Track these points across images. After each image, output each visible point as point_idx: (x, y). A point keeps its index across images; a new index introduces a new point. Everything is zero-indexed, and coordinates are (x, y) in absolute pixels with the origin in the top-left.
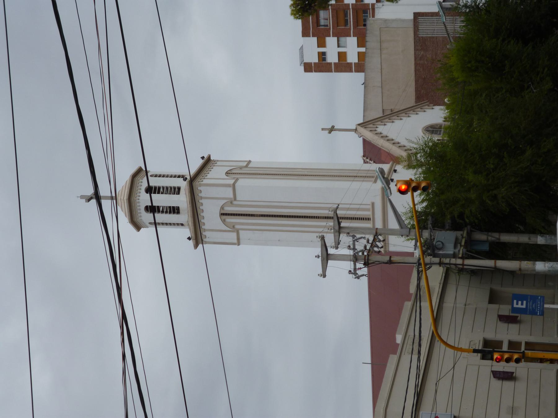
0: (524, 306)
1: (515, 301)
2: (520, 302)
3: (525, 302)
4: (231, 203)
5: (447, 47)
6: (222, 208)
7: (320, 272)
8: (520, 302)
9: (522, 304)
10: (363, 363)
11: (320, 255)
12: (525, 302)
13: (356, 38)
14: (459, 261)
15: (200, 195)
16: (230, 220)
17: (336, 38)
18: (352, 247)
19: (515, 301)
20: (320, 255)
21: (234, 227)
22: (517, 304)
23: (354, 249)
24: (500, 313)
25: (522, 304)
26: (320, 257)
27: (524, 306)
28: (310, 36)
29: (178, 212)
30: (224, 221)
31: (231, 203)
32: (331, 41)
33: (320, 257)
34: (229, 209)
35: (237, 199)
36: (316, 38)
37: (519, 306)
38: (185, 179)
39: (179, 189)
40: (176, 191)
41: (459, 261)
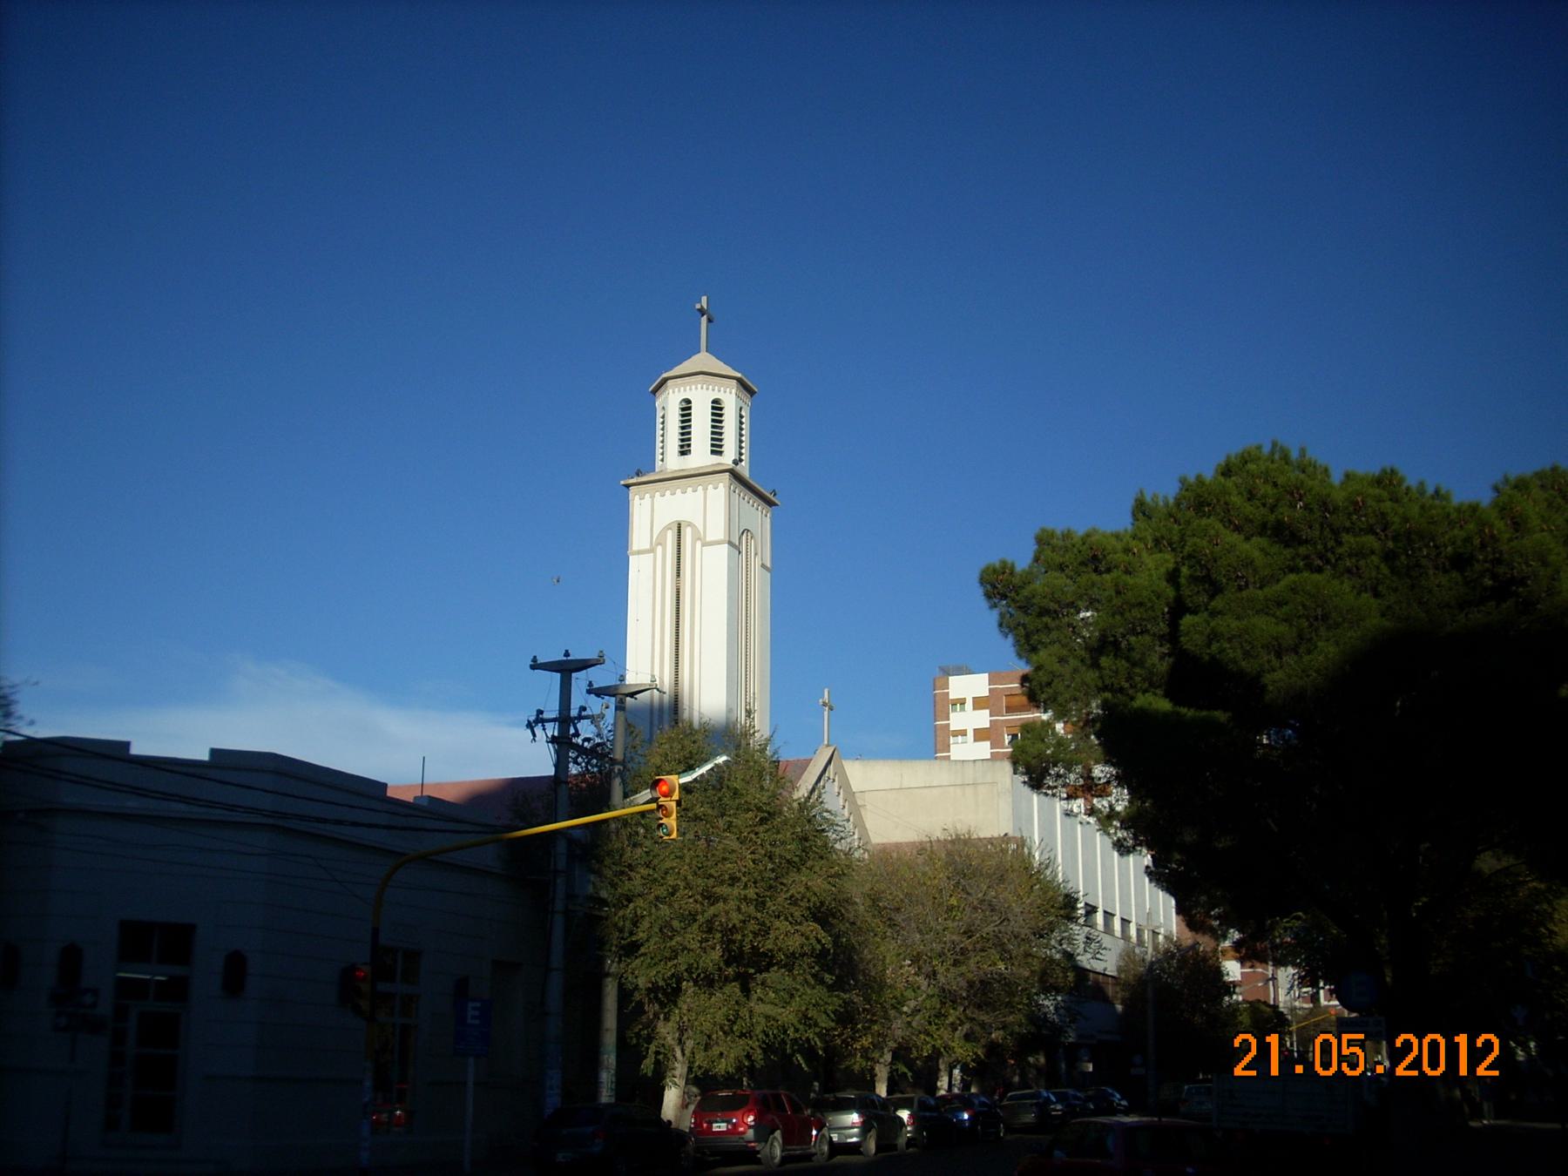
0: (469, 1021)
1: (478, 1005)
2: (477, 1013)
3: (477, 1022)
4: (697, 537)
5: (1029, 1063)
6: (690, 524)
7: (541, 660)
8: (477, 1013)
9: (474, 1017)
10: (424, 758)
11: (569, 658)
12: (477, 1022)
13: (988, 725)
14: (559, 906)
15: (710, 487)
16: (671, 537)
17: (989, 757)
18: (584, 713)
19: (478, 1005)
20: (569, 658)
21: (660, 544)
22: (474, 1009)
23: (580, 718)
24: (1106, 909)
25: (474, 1017)
26: (565, 658)
27: (469, 1021)
28: (990, 685)
29: (683, 453)
30: (668, 527)
31: (699, 539)
32: (983, 719)
33: (565, 658)
34: (688, 534)
35: (704, 548)
36: (987, 694)
37: (471, 1013)
38: (736, 462)
39: (720, 453)
40: (717, 449)
41: (559, 906)
